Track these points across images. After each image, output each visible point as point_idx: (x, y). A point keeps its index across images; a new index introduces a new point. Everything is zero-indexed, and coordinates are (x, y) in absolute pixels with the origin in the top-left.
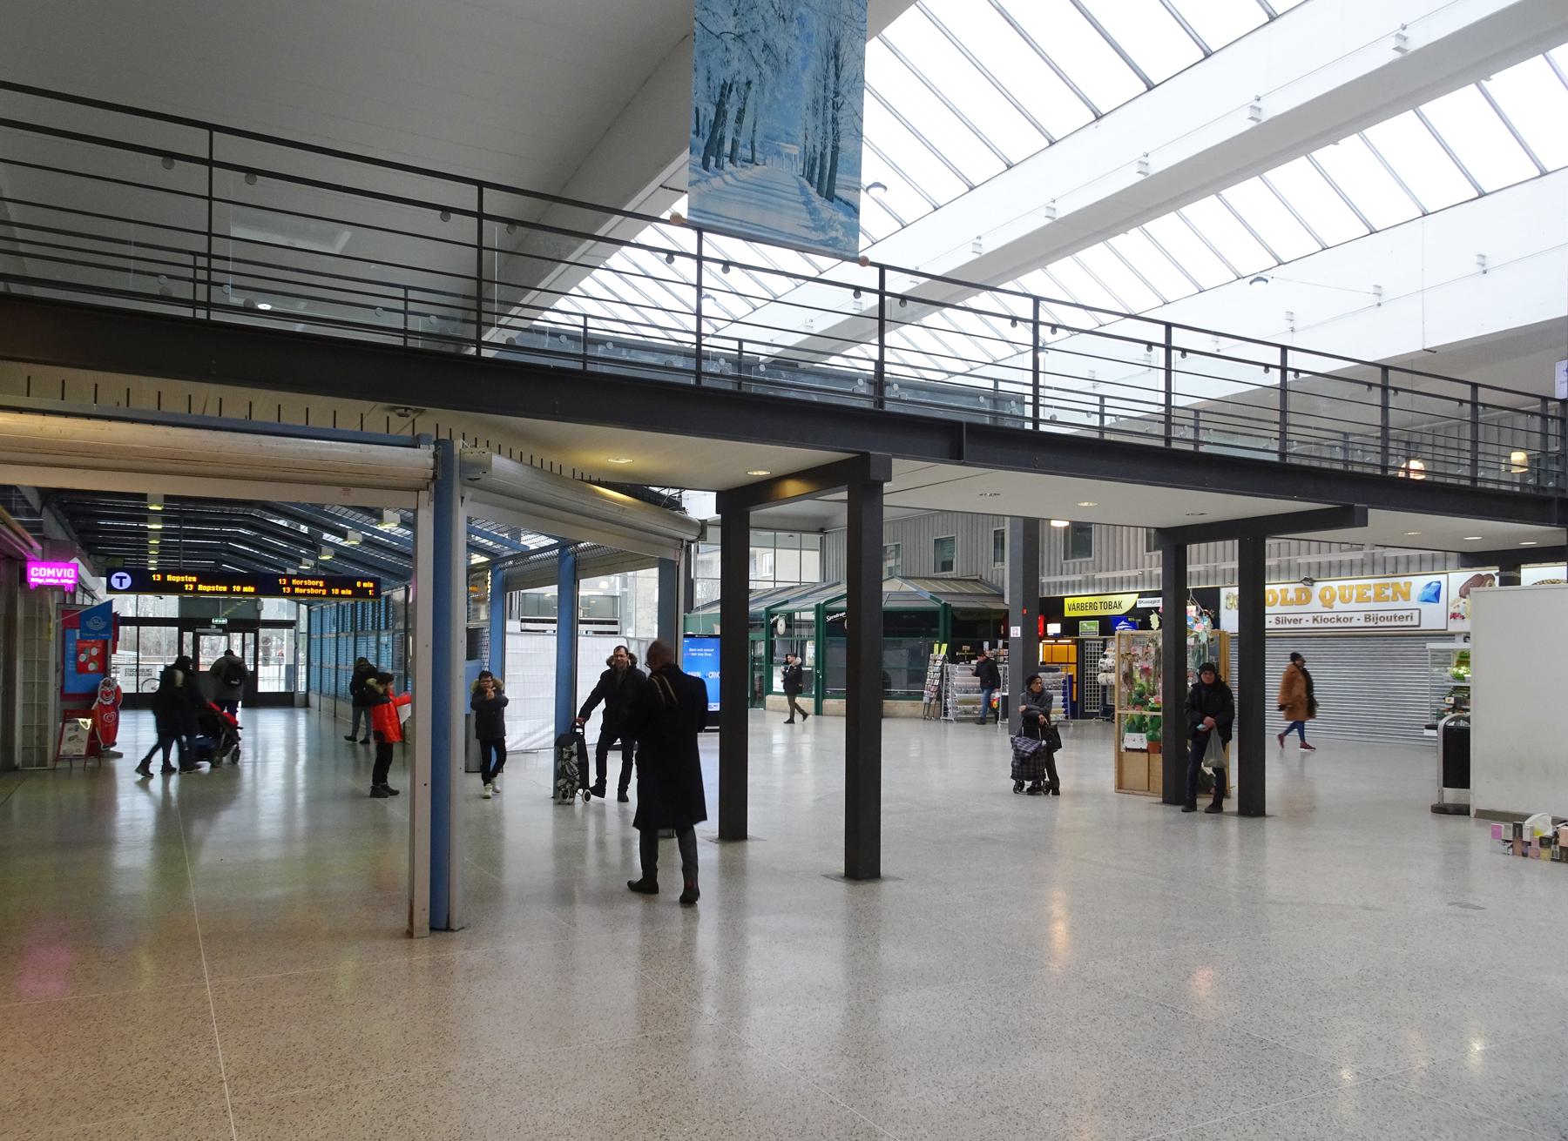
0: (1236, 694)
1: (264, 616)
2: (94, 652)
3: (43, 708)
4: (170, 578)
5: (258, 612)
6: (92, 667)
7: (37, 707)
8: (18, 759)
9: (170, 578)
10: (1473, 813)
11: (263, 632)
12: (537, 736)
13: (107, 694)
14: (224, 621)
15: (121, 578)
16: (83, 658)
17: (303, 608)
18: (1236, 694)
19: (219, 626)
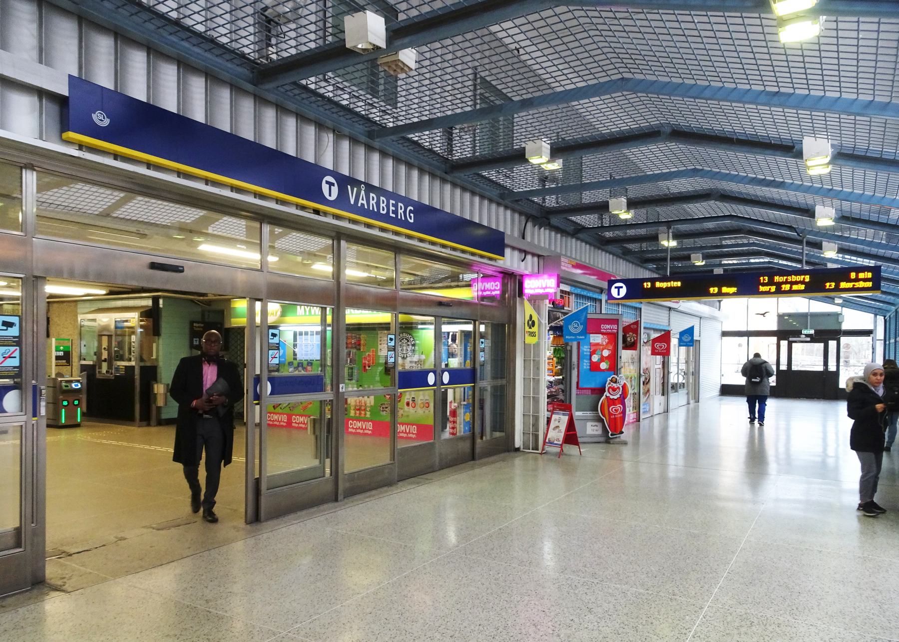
0: (203, 462)
1: (845, 327)
2: (606, 353)
3: (536, 401)
4: (658, 285)
5: (840, 323)
6: (604, 366)
7: (532, 400)
8: (518, 442)
9: (658, 285)
10: (499, 382)
11: (844, 340)
12: (334, 440)
13: (614, 390)
14: (812, 332)
15: (619, 288)
16: (595, 358)
17: (881, 319)
18: (203, 462)
19: (807, 336)
